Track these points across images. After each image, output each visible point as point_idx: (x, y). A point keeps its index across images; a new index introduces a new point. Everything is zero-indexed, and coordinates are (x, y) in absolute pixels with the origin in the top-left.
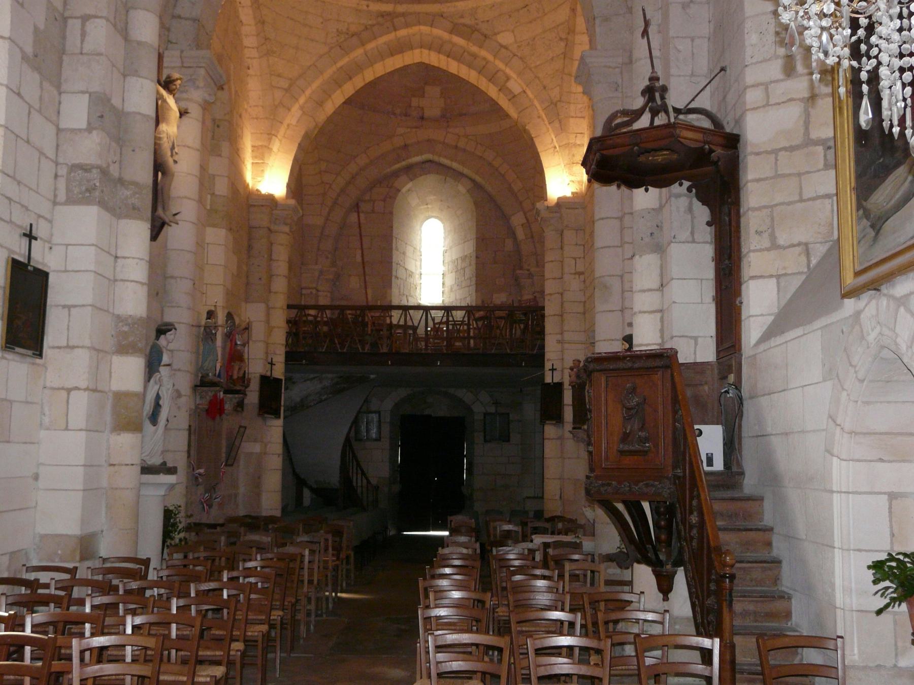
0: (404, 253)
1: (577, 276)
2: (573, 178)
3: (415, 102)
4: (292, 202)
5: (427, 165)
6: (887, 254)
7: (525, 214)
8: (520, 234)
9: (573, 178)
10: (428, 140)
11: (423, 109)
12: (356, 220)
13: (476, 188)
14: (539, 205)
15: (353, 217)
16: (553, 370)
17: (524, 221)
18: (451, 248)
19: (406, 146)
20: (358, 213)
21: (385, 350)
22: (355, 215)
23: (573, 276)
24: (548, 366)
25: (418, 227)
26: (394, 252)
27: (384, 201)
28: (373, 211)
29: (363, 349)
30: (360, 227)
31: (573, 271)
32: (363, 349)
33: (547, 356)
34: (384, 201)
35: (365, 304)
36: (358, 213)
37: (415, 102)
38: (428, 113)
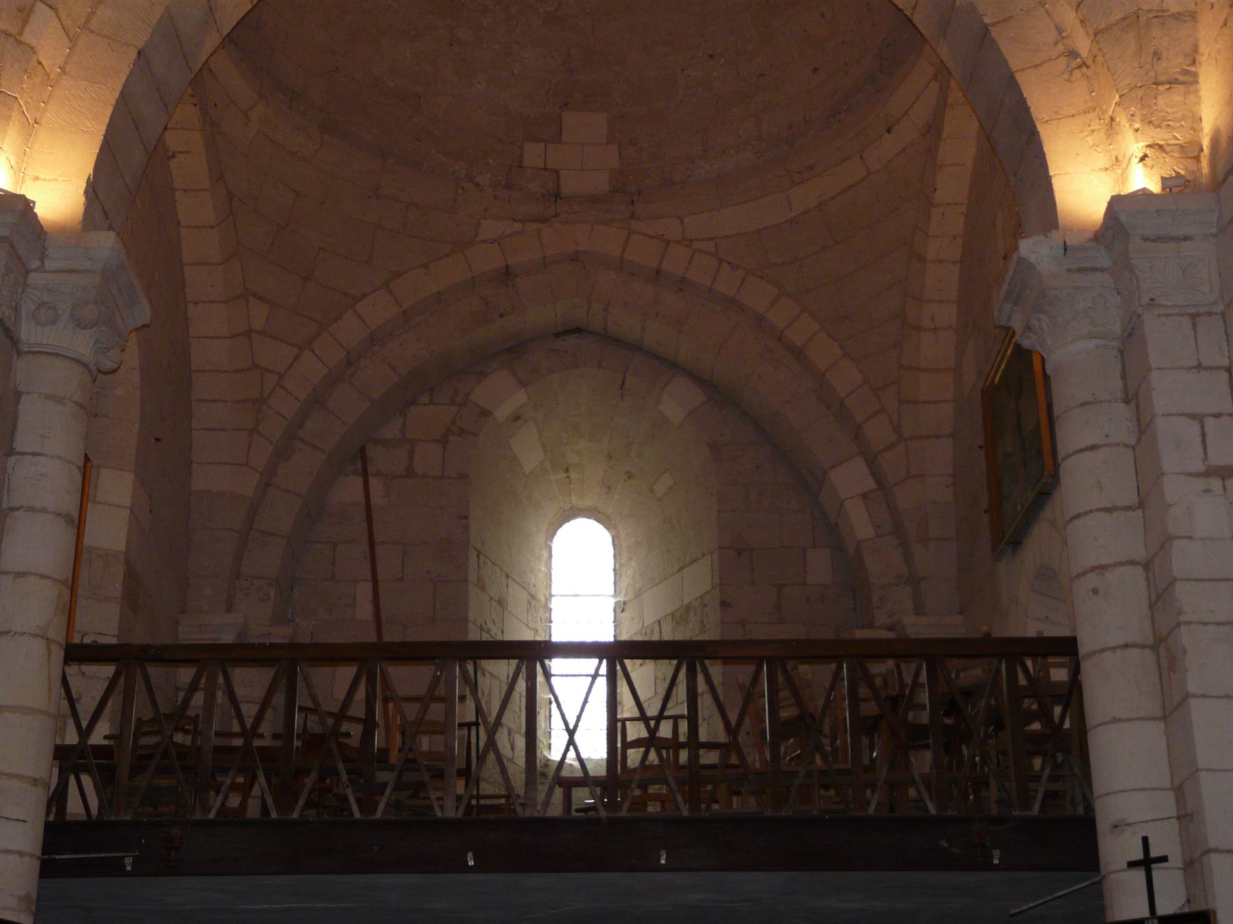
0: (501, 603)
1: (1216, 483)
2: (1160, 136)
3: (533, 154)
4: (106, 243)
5: (572, 340)
6: (1156, 888)
7: (872, 462)
8: (860, 523)
9: (1160, 136)
10: (575, 258)
11: (557, 172)
12: (361, 499)
13: (720, 395)
14: (1035, 250)
15: (349, 490)
16: (1147, 863)
17: (871, 484)
18: (638, 595)
19: (507, 275)
20: (365, 475)
21: (449, 811)
22: (358, 482)
23: (1200, 484)
24: (1117, 850)
25: (540, 538)
26: (473, 590)
27: (443, 441)
28: (410, 473)
29: (367, 805)
30: (369, 516)
31: (1201, 467)
32: (367, 805)
33: (1108, 811)
34: (443, 441)
35: (372, 637)
36: (365, 475)
37: (533, 154)
38: (571, 185)
